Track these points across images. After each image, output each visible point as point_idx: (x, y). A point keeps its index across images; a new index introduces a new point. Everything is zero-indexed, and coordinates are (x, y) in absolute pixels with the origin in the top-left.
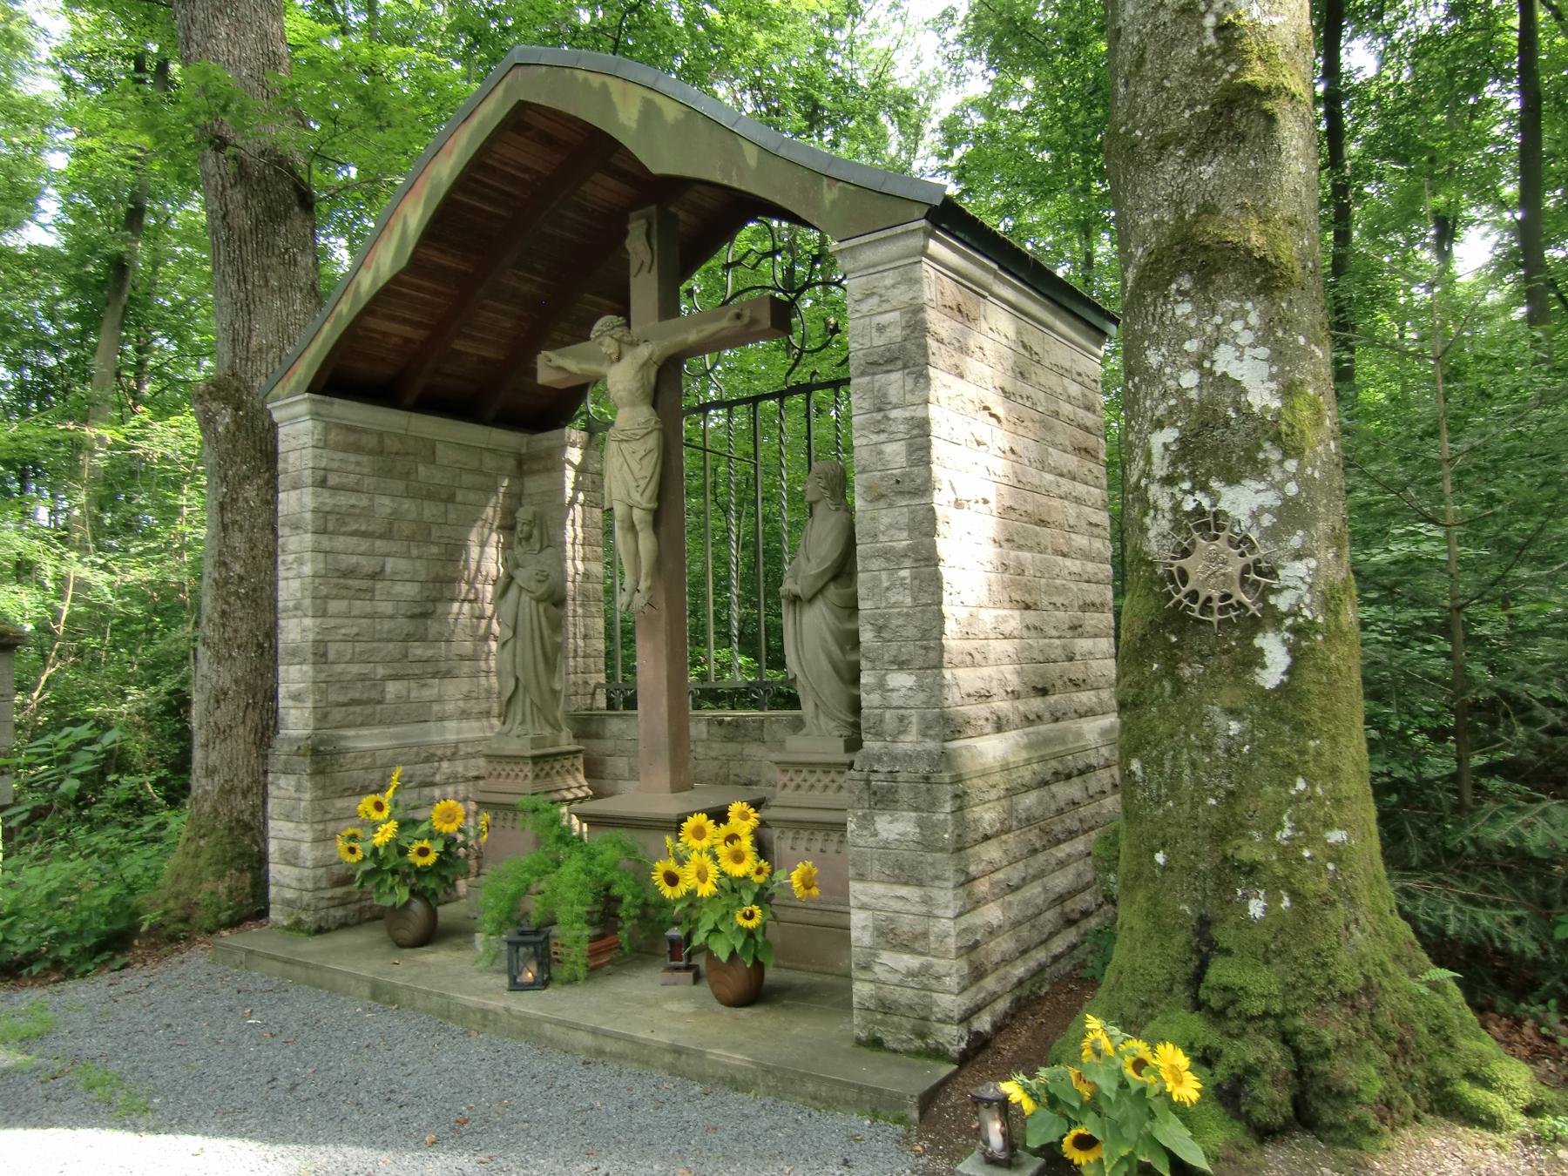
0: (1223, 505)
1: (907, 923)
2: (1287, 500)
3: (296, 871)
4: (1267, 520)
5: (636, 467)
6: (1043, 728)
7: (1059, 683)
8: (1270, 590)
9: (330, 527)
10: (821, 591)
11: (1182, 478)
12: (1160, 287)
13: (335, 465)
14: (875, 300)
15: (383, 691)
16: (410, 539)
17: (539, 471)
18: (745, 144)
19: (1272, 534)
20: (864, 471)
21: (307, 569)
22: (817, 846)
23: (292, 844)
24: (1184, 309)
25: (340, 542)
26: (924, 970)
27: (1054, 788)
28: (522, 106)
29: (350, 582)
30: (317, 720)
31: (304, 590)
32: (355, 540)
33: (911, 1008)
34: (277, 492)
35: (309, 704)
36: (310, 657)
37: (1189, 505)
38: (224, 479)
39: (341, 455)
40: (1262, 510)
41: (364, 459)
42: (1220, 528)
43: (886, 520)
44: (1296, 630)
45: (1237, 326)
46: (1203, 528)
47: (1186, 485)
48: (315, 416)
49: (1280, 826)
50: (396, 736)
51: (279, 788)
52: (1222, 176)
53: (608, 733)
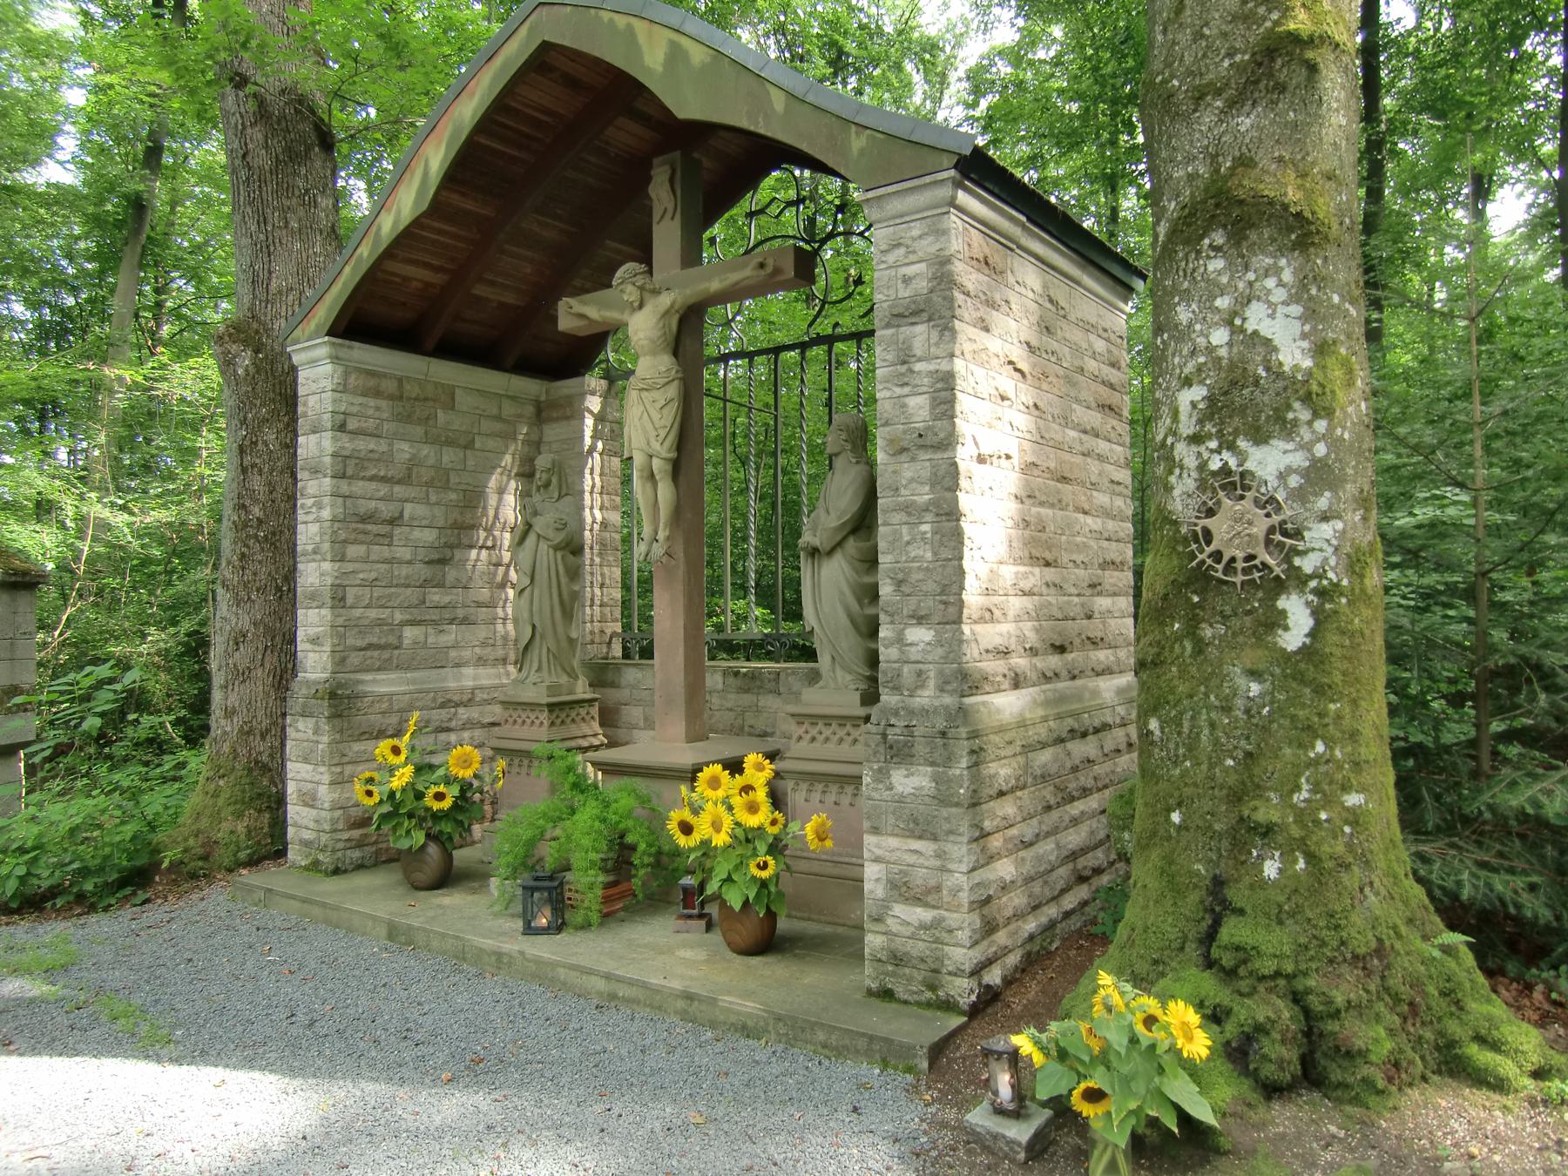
0: (1250, 465)
1: (920, 877)
2: (1315, 461)
3: (314, 812)
4: (1294, 481)
5: (656, 416)
6: (1060, 685)
7: (1077, 641)
10: (839, 544)
11: (1209, 436)
12: (1192, 242)
13: (354, 409)
14: (902, 250)
17: (557, 419)
18: (773, 91)
19: (1299, 495)
20: (886, 424)
21: (326, 514)
23: (310, 786)
24: (1217, 264)
25: (359, 487)
26: (936, 924)
27: (1069, 745)
28: (546, 46)
29: (369, 527)
30: (334, 664)
32: (374, 485)
33: (922, 960)
37: (1215, 465)
39: (360, 400)
40: (1290, 470)
41: (383, 403)
43: (908, 474)
44: (1321, 593)
45: (1270, 283)
47: (1213, 444)
48: (335, 359)
49: (1298, 788)
52: (1261, 129)
53: (623, 682)
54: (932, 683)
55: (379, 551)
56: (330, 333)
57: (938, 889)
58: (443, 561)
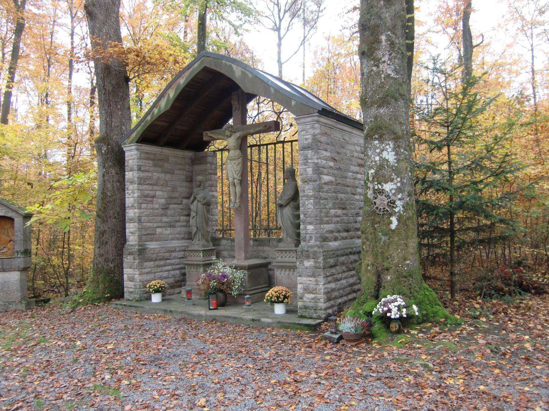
0: (384, 188)
3: (133, 283)
4: (393, 191)
5: (235, 167)
6: (347, 240)
7: (352, 229)
8: (393, 207)
9: (142, 183)
13: (143, 164)
14: (305, 132)
15: (156, 231)
16: (162, 185)
19: (394, 194)
21: (136, 195)
22: (287, 272)
23: (132, 275)
24: (377, 142)
25: (144, 187)
27: (350, 256)
28: (205, 67)
29: (147, 199)
30: (139, 239)
31: (134, 201)
32: (148, 186)
33: (312, 307)
34: (125, 172)
35: (137, 235)
36: (137, 221)
37: (376, 188)
38: (104, 167)
39: (144, 161)
40: (392, 189)
41: (150, 162)
42: (383, 193)
43: (307, 188)
45: (388, 147)
46: (380, 193)
48: (137, 150)
50: (158, 245)
51: (127, 259)
52: (385, 113)
53: (221, 244)
54: (313, 239)
55: (150, 206)
56: (137, 142)
57: (316, 289)
58: (166, 209)
